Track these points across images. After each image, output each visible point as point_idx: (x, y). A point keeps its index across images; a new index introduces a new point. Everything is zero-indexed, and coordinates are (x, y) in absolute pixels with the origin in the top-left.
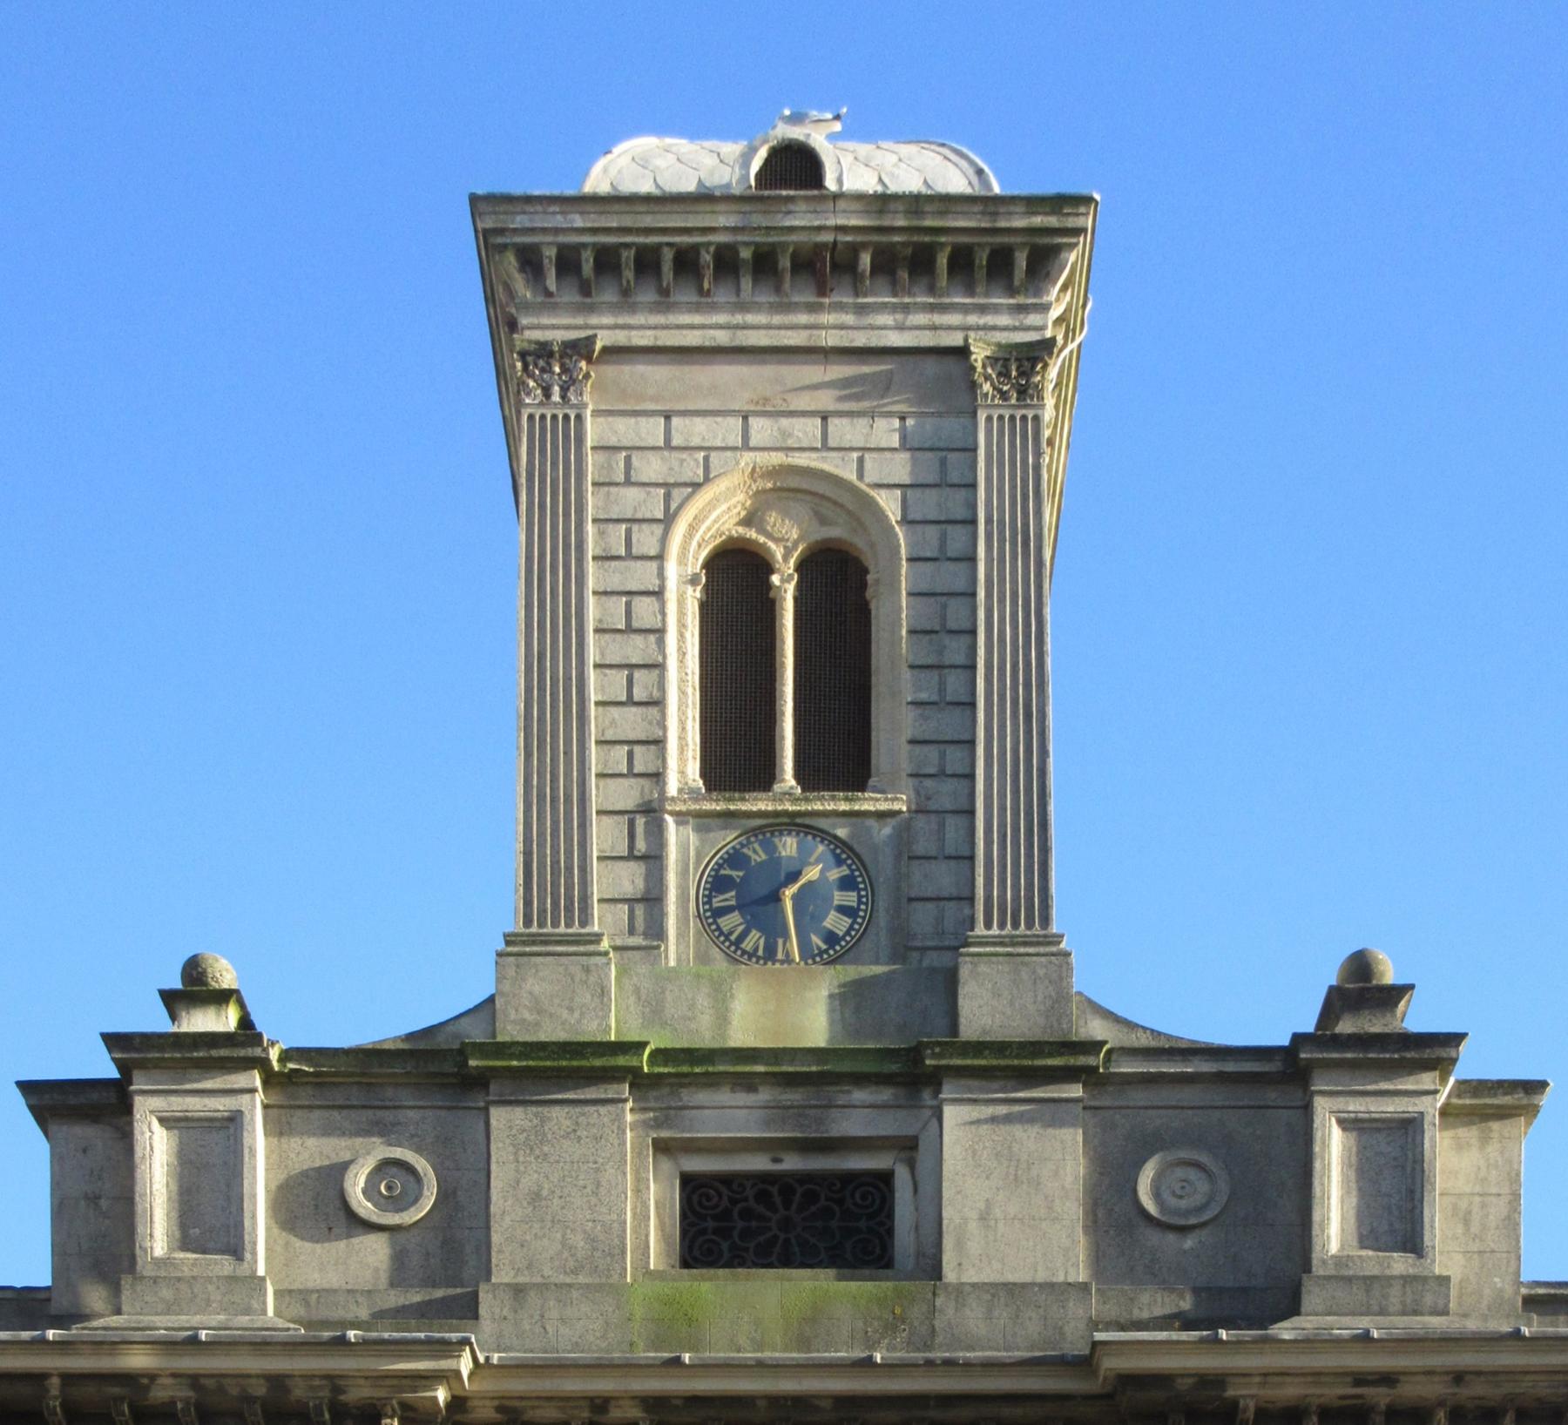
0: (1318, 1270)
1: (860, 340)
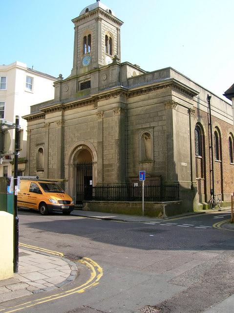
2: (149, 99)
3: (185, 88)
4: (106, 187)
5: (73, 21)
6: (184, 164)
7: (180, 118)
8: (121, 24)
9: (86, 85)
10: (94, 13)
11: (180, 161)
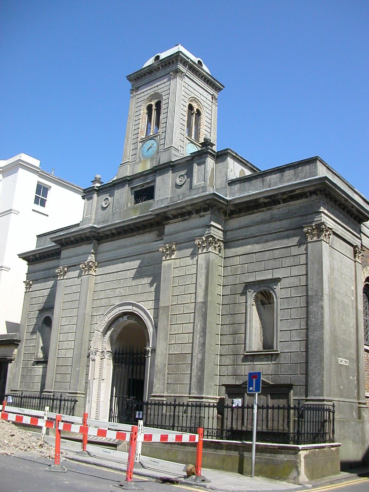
0: (193, 188)
1: (161, 75)
2: (272, 219)
3: (346, 201)
4: (57, 399)
5: (129, 78)
6: (343, 361)
7: (335, 262)
8: (220, 89)
9: (145, 194)
10: (169, 63)
11: (335, 353)
